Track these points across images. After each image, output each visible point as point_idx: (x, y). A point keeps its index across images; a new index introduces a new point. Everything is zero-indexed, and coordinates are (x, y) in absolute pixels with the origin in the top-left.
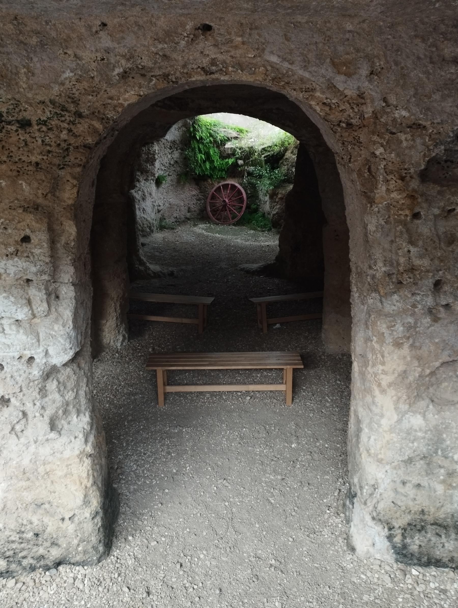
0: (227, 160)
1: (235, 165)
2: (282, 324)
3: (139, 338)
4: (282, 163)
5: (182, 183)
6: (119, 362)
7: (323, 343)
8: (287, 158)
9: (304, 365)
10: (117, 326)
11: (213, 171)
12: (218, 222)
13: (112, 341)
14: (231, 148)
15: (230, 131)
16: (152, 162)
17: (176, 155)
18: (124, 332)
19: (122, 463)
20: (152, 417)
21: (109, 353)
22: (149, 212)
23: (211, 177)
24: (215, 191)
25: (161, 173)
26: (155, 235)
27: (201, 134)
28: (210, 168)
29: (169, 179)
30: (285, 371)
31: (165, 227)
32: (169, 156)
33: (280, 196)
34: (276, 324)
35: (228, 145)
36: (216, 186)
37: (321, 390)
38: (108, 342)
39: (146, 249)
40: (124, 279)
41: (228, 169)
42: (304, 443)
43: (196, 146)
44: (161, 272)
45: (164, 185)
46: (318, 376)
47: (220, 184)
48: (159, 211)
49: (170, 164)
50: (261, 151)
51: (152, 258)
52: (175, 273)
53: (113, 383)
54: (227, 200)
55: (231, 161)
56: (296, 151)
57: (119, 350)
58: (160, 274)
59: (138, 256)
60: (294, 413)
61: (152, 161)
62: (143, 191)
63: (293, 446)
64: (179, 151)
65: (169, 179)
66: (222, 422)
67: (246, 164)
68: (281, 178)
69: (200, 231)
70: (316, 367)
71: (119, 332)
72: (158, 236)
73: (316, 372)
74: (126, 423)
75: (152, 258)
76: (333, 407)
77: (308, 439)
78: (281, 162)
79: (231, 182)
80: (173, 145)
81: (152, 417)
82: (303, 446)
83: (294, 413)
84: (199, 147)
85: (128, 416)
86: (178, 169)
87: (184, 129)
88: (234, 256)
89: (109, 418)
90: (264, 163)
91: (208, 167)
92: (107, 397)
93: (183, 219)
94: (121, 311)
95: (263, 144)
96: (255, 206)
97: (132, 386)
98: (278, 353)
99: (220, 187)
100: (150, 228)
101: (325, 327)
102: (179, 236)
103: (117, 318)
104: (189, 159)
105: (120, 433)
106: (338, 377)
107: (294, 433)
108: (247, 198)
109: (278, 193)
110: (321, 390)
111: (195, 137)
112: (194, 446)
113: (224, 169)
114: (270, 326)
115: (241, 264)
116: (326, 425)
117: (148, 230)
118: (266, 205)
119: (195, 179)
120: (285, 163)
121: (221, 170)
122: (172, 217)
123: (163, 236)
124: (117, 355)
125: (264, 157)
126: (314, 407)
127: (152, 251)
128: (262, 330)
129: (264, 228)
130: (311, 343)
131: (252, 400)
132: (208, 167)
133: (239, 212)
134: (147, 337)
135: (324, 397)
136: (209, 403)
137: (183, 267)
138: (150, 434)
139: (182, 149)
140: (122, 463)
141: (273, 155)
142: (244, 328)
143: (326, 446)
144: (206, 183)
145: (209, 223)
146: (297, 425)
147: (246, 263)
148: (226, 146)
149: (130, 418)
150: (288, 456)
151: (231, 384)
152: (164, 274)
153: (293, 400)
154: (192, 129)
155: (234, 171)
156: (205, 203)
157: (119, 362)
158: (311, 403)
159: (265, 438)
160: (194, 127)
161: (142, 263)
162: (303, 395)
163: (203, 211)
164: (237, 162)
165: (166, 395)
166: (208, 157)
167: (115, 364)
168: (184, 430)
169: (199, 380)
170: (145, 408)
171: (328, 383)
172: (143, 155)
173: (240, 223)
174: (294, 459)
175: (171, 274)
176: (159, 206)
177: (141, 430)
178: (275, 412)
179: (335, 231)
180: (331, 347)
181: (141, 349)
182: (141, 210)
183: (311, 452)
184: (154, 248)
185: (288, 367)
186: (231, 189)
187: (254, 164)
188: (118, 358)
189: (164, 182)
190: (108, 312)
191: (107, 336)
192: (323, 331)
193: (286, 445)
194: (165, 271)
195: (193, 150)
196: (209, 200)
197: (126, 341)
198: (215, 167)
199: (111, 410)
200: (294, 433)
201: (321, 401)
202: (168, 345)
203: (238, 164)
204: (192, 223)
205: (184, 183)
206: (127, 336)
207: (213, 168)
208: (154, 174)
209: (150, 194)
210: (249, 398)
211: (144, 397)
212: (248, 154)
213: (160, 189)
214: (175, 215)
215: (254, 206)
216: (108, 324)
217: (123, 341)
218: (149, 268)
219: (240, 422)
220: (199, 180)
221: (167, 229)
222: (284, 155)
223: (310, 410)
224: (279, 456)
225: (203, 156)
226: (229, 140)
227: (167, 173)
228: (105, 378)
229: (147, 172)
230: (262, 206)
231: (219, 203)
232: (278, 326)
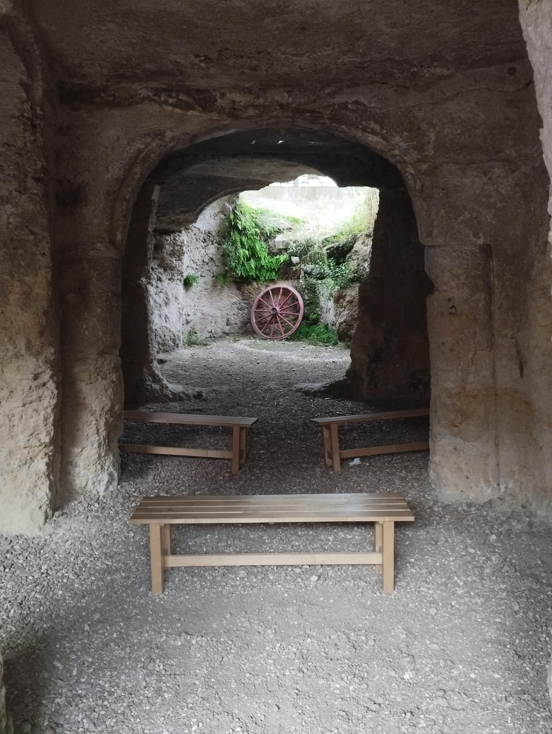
0: (278, 257)
1: (289, 264)
2: (362, 458)
3: (138, 481)
4: (350, 257)
5: (219, 287)
6: (98, 517)
7: (433, 486)
8: (356, 251)
9: (414, 515)
10: (100, 457)
11: (260, 271)
12: (266, 336)
13: (90, 483)
14: (283, 242)
15: (282, 221)
16: (179, 257)
17: (212, 250)
18: (111, 469)
19: (61, 714)
20: (137, 614)
21: (83, 502)
22: (174, 321)
23: (257, 279)
24: (262, 297)
25: (191, 272)
26: (180, 351)
27: (245, 222)
28: (256, 267)
29: (201, 281)
30: (378, 528)
31: (195, 343)
32: (203, 251)
33: (348, 299)
34: (353, 459)
35: (279, 238)
36: (264, 290)
37: (442, 564)
38: (84, 483)
39: (166, 366)
40: (113, 382)
41: (279, 269)
42: (427, 669)
43: (238, 239)
44: (184, 393)
45: (196, 287)
46: (433, 539)
47: (269, 289)
48: (188, 323)
49: (203, 262)
50: (323, 242)
51: (174, 377)
52: (204, 395)
53: (81, 552)
54: (278, 309)
55: (283, 258)
56: (370, 242)
57: (101, 498)
58: (182, 395)
59: (150, 369)
60: (401, 608)
61: (178, 254)
62: (166, 294)
63: (406, 676)
64: (216, 245)
65: (201, 281)
66: (268, 626)
67: (302, 261)
68: (350, 276)
69: (242, 347)
70: (426, 525)
71: (102, 468)
72: (184, 354)
73: (428, 532)
74: (87, 628)
75: (174, 377)
76: (470, 597)
77: (435, 661)
78: (348, 255)
79: (282, 284)
80: (208, 237)
81: (137, 614)
82: (426, 676)
83: (401, 608)
84: (241, 240)
85: (94, 612)
86: (215, 268)
87: (222, 216)
88: (286, 378)
89: (58, 616)
90: (326, 258)
92: (63, 577)
93: (220, 334)
94: (108, 435)
95: (325, 234)
96: (315, 315)
97: (111, 557)
98: (364, 496)
99: (268, 292)
100: (174, 341)
101: (436, 458)
102: (214, 353)
103: (99, 445)
104: (228, 255)
105: (71, 648)
106: (469, 541)
107: (405, 650)
108: (305, 306)
109: (345, 295)
110: (441, 563)
111: (235, 227)
112: (208, 677)
113: (274, 269)
114: (344, 461)
115: (297, 383)
116: (463, 632)
117: (171, 343)
118: (331, 314)
119: (236, 282)
120: (354, 257)
121: (271, 270)
122: (205, 331)
123: (191, 352)
124: (96, 505)
125: (327, 250)
126: (435, 596)
127: (175, 369)
128: (332, 467)
129: (327, 342)
130: (413, 486)
131: (320, 582)
133: (294, 324)
134: (150, 478)
135: (450, 578)
136: (244, 587)
137: (216, 388)
138: (128, 650)
139: (219, 244)
140: (61, 714)
141: (338, 247)
142: (304, 465)
143: (473, 676)
144: (250, 287)
145: (254, 338)
146: (408, 631)
147: (305, 382)
148: (276, 240)
149: (97, 616)
150: (399, 699)
151: (284, 551)
152: (187, 395)
153: (395, 583)
154: (232, 217)
155: (286, 271)
156: (249, 313)
157: (98, 517)
158: (429, 589)
159: (349, 659)
160: (235, 214)
161: (156, 379)
162: (412, 573)
163: (247, 324)
164: (290, 259)
165: (166, 572)
166: (253, 254)
167: (90, 520)
168: (194, 642)
169: (229, 546)
170: (128, 596)
171: (453, 550)
172: (167, 246)
173: (295, 337)
174: (412, 706)
175: (199, 396)
176: (189, 315)
177: (114, 640)
178: (364, 606)
179: (449, 300)
180: (448, 492)
181: (137, 497)
182: (163, 318)
183: (445, 691)
184: (178, 366)
185: (387, 518)
186: (282, 295)
187: (314, 260)
188: (97, 511)
189: (195, 284)
190: (85, 434)
191: (82, 474)
192: (432, 466)
193: (393, 674)
194: (190, 392)
195: (234, 243)
196: (254, 309)
197: (115, 483)
198: (262, 266)
199: (65, 599)
200: (405, 650)
201: (446, 585)
202: (183, 491)
204: (232, 339)
205: (222, 287)
206: (116, 475)
207: (259, 268)
208: (182, 273)
209: (176, 298)
210: (314, 578)
211: (128, 578)
212: (304, 251)
213: (190, 293)
214: (209, 329)
215: (313, 316)
216: (85, 453)
217: (110, 482)
218: (167, 387)
219: (299, 625)
220: (242, 283)
221: (198, 345)
222: (352, 247)
223: (430, 602)
224: (380, 700)
225: (247, 252)
226: (279, 231)
227: (200, 273)
228: (69, 543)
229: (172, 269)
230: (324, 315)
231: (267, 314)
232: (357, 461)
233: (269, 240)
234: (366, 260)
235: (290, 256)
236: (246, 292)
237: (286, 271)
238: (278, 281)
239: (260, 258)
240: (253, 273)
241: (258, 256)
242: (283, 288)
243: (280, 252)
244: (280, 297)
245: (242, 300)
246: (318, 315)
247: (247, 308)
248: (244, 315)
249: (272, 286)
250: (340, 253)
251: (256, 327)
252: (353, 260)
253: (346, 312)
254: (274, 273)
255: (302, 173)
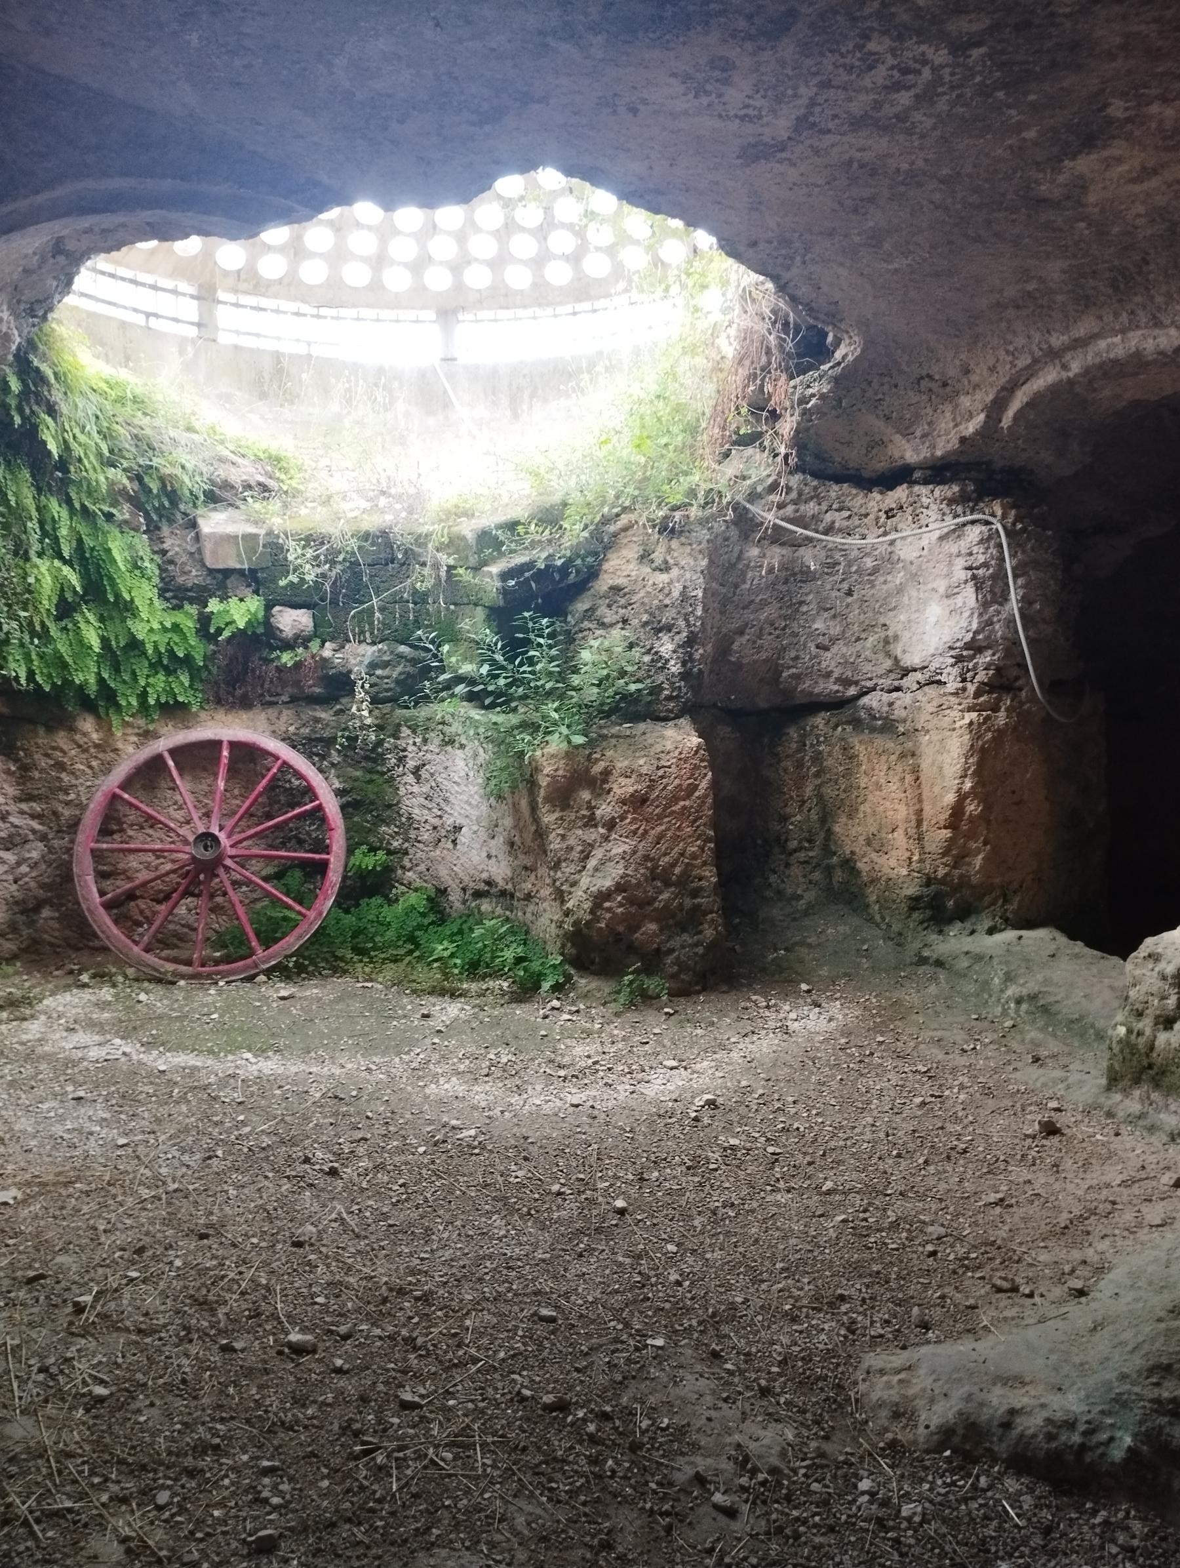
1: (261, 637)
8: (616, 589)
23: (103, 702)
33: (623, 787)
36: (132, 755)
47: (162, 745)
55: (240, 610)
78: (581, 606)
79: (227, 728)
91: (93, 638)
109: (607, 773)
121: (169, 663)
125: (505, 576)
132: (93, 638)
144: (61, 739)
164: (267, 622)
166: (97, 588)
198: (135, 645)
203: (270, 629)
207: (122, 653)
222: (593, 574)
233: (166, 530)
234: (668, 628)
235: (269, 607)
236: (43, 763)
237: (242, 670)
238: (203, 715)
239: (127, 609)
240: (87, 676)
241: (118, 596)
242: (233, 745)
243: (222, 581)
244: (221, 784)
245: (17, 800)
246: (390, 853)
247: (43, 838)
248: (24, 869)
249: (171, 737)
250: (548, 595)
251: (104, 922)
252: (603, 625)
253: (619, 848)
254: (185, 679)
255: (404, 204)
